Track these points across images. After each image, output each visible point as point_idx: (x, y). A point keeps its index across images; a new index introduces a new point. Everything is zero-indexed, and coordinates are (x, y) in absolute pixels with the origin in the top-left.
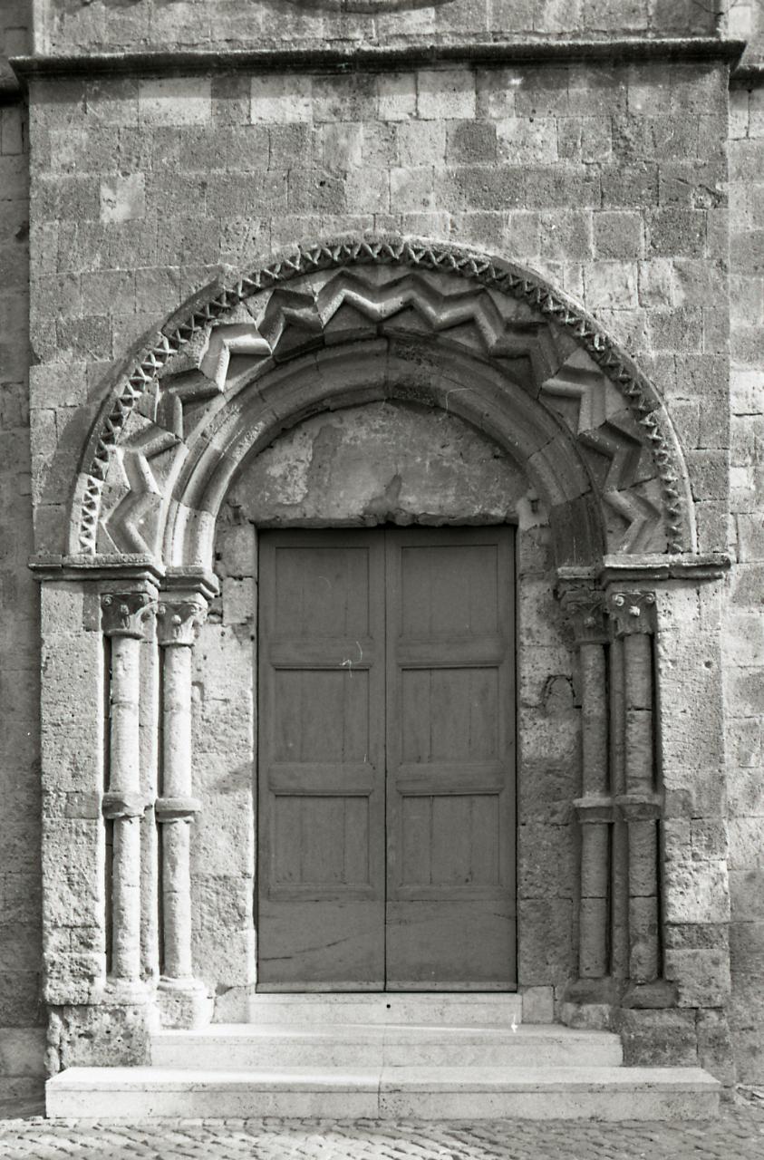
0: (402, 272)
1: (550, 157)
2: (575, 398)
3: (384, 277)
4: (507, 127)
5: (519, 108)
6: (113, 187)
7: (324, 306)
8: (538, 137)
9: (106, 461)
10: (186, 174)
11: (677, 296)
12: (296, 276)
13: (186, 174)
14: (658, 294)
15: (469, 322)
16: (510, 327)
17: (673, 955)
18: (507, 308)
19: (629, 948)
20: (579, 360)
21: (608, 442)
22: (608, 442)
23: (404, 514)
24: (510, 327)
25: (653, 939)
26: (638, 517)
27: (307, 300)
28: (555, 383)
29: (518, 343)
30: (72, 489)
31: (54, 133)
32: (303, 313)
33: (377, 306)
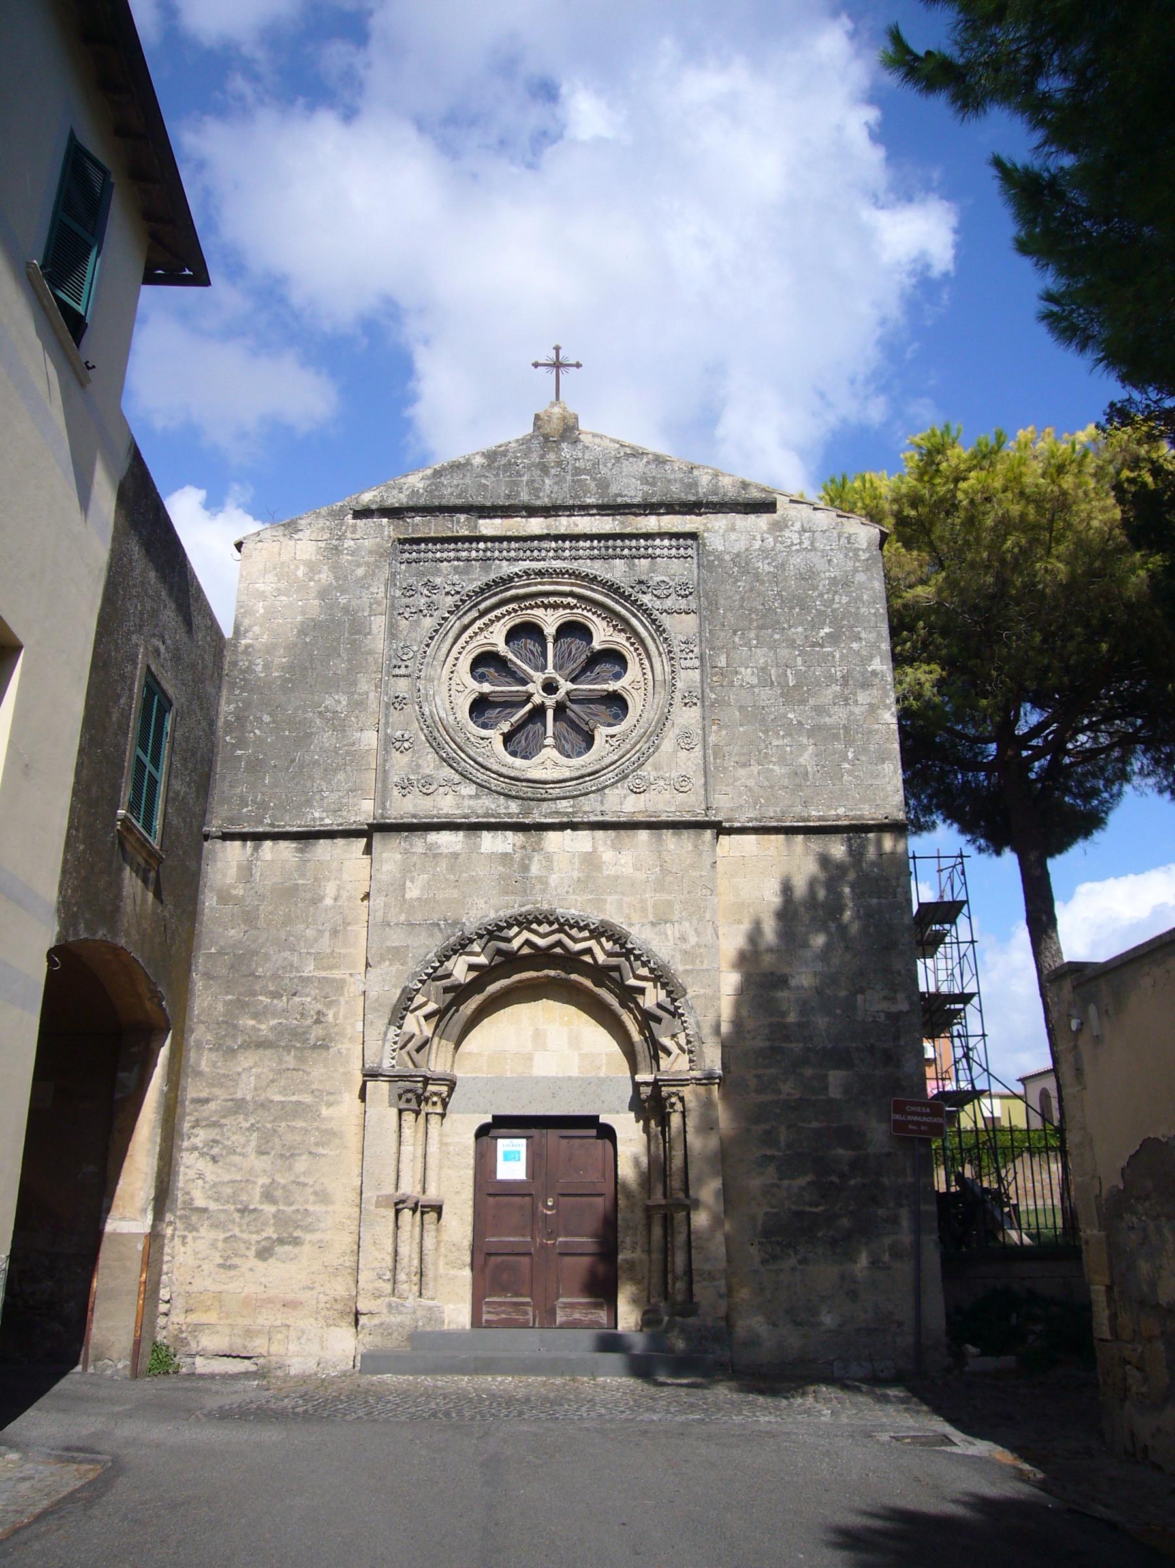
0: (556, 926)
1: (628, 870)
2: (642, 991)
3: (545, 928)
4: (608, 855)
5: (614, 847)
6: (412, 882)
7: (517, 941)
8: (623, 861)
9: (332, 1203)
10: (393, 1319)
11: (693, 940)
12: (501, 929)
13: (393, 1319)
14: (683, 939)
15: (589, 951)
16: (609, 954)
17: (696, 1288)
18: (608, 945)
19: (674, 1284)
20: (644, 972)
21: (660, 1013)
22: (660, 1013)
23: (213, 691)
24: (609, 954)
25: (686, 1278)
26: (675, 1050)
27: (509, 940)
28: (632, 982)
29: (614, 961)
30: (385, 1034)
31: (385, 855)
32: (503, 945)
33: (541, 942)
